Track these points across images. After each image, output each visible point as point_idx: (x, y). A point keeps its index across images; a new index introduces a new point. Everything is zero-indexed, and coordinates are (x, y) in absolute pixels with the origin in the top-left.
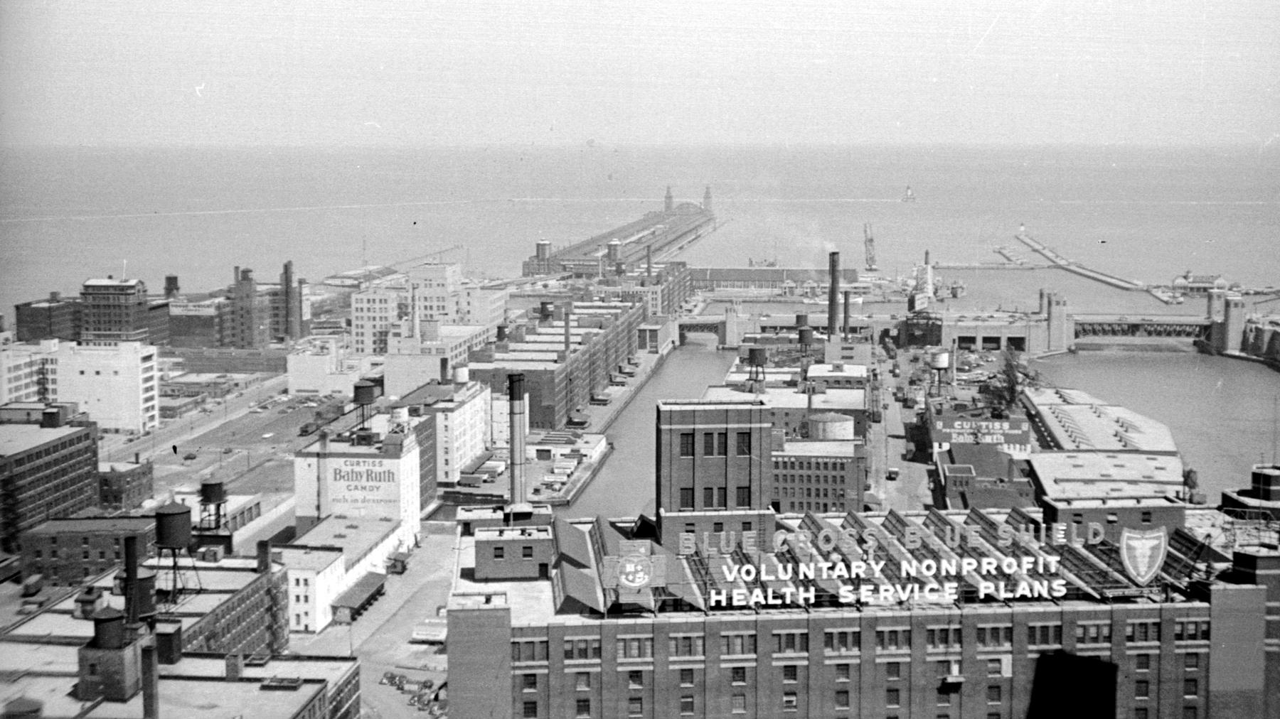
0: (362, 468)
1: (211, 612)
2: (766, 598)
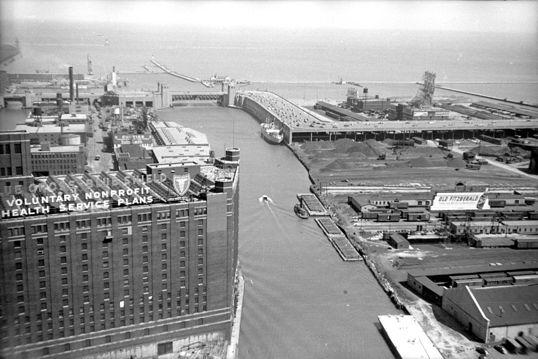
2: (28, 212)
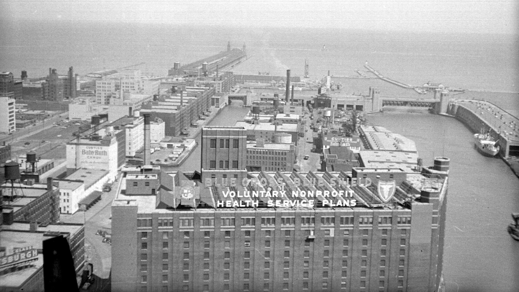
0: (94, 150)
1: (27, 205)
2: (239, 204)
